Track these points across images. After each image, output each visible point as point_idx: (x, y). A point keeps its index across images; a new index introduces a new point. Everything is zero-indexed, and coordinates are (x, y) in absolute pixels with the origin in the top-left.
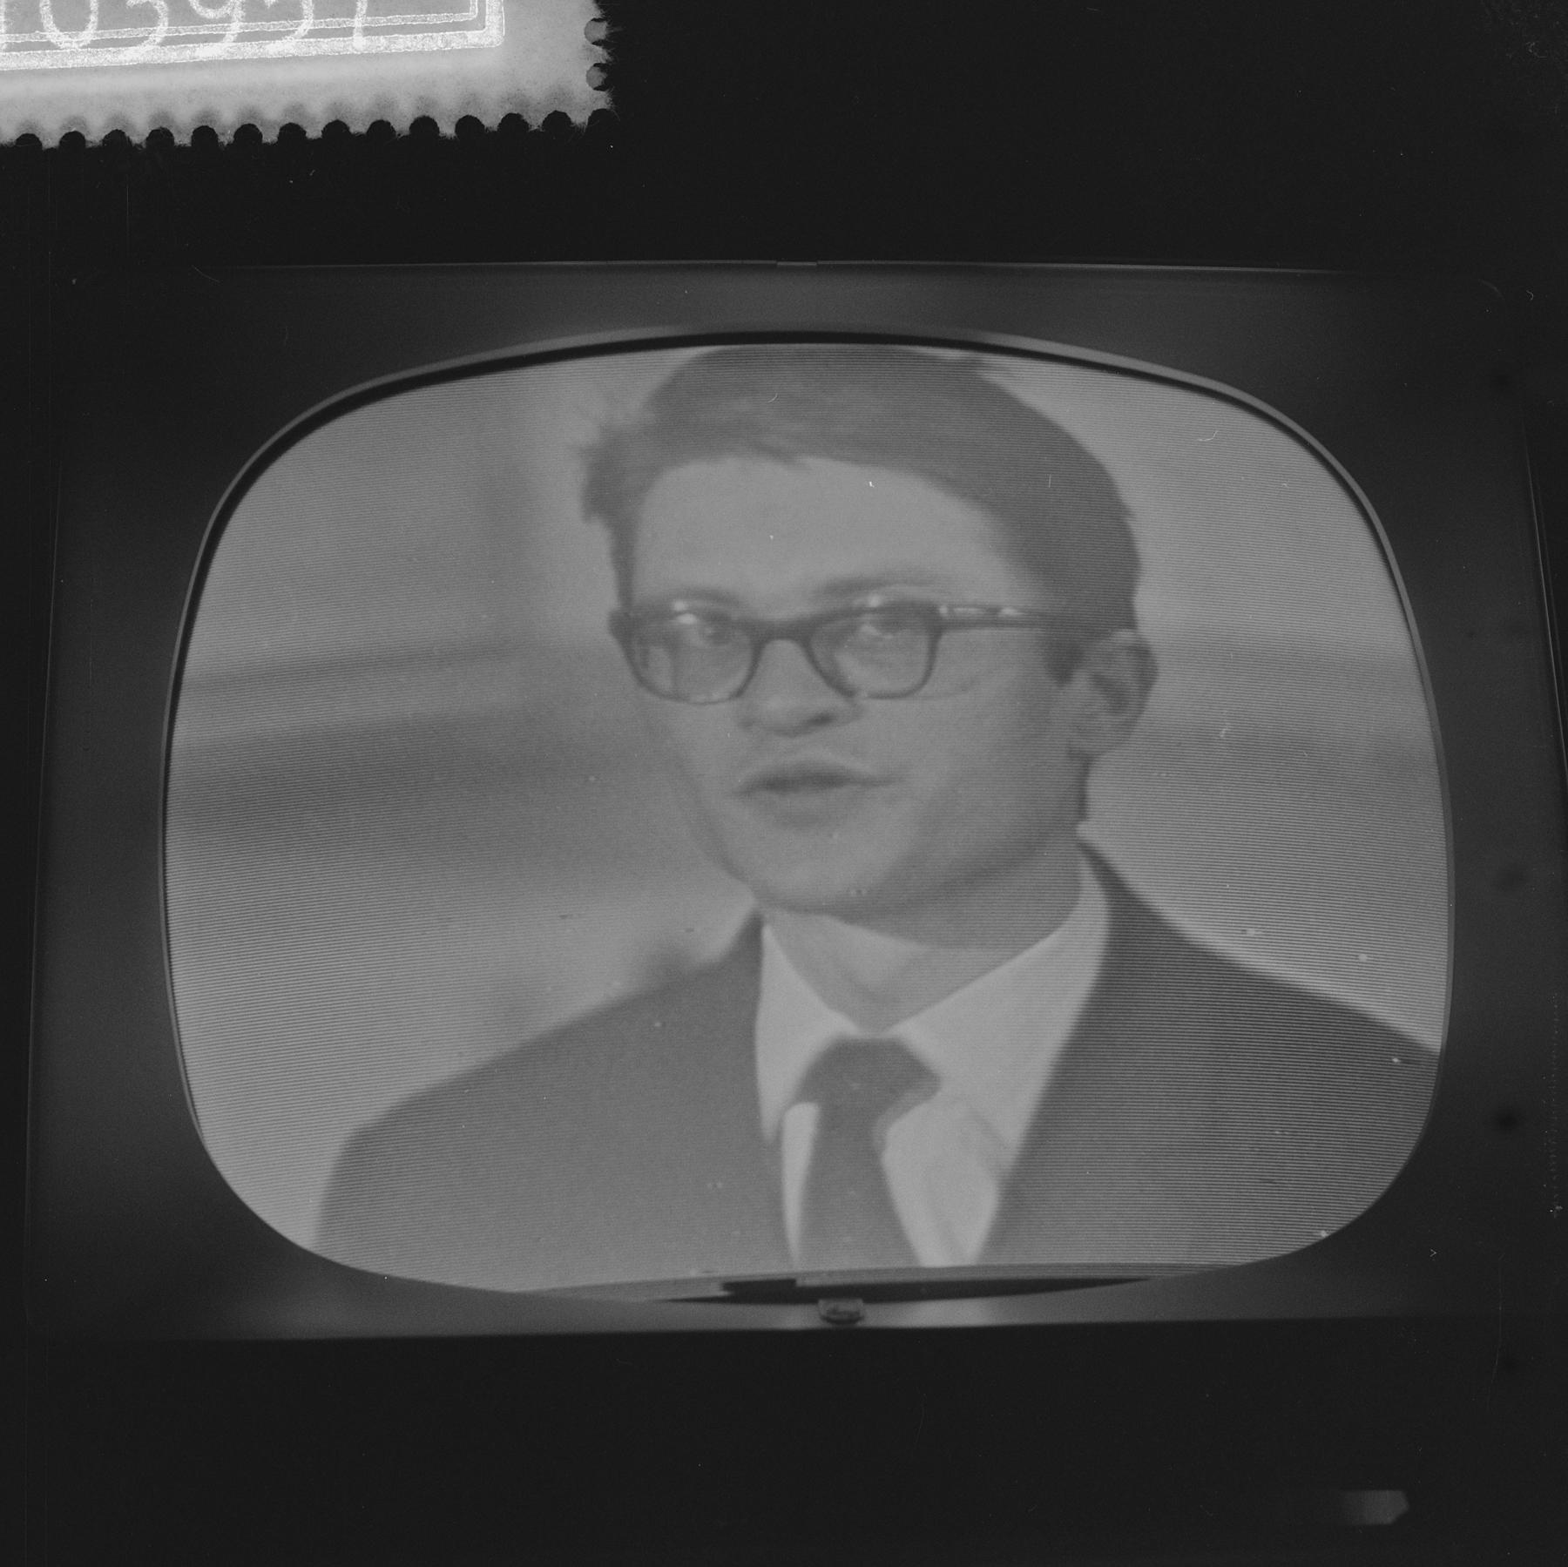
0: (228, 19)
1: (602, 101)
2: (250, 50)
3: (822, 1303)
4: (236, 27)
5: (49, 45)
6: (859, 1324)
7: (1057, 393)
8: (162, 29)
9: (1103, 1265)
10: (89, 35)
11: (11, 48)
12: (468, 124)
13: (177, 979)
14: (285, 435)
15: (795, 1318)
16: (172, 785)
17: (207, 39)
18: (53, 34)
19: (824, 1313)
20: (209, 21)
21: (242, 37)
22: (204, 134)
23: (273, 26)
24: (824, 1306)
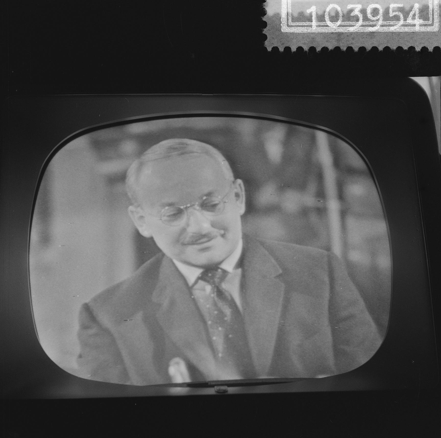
0: (378, 20)
1: (264, 32)
2: (386, 29)
3: (215, 387)
4: (380, 22)
5: (327, 26)
6: (226, 393)
7: (246, 127)
8: (361, 22)
9: (306, 378)
10: (339, 23)
11: (319, 26)
12: (362, 49)
13: (33, 296)
14: (78, 133)
15: (211, 391)
16: (31, 241)
17: (371, 26)
18: (329, 23)
19: (216, 390)
20: (373, 21)
21: (382, 26)
22: (312, 49)
23: (392, 23)
24: (216, 388)
